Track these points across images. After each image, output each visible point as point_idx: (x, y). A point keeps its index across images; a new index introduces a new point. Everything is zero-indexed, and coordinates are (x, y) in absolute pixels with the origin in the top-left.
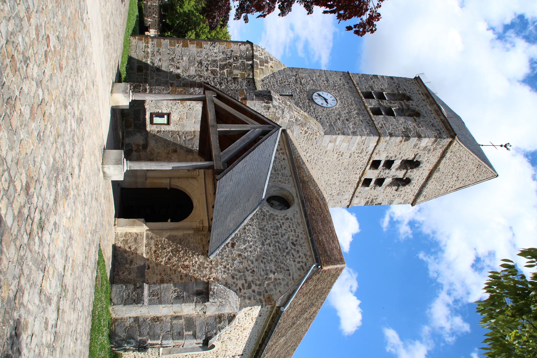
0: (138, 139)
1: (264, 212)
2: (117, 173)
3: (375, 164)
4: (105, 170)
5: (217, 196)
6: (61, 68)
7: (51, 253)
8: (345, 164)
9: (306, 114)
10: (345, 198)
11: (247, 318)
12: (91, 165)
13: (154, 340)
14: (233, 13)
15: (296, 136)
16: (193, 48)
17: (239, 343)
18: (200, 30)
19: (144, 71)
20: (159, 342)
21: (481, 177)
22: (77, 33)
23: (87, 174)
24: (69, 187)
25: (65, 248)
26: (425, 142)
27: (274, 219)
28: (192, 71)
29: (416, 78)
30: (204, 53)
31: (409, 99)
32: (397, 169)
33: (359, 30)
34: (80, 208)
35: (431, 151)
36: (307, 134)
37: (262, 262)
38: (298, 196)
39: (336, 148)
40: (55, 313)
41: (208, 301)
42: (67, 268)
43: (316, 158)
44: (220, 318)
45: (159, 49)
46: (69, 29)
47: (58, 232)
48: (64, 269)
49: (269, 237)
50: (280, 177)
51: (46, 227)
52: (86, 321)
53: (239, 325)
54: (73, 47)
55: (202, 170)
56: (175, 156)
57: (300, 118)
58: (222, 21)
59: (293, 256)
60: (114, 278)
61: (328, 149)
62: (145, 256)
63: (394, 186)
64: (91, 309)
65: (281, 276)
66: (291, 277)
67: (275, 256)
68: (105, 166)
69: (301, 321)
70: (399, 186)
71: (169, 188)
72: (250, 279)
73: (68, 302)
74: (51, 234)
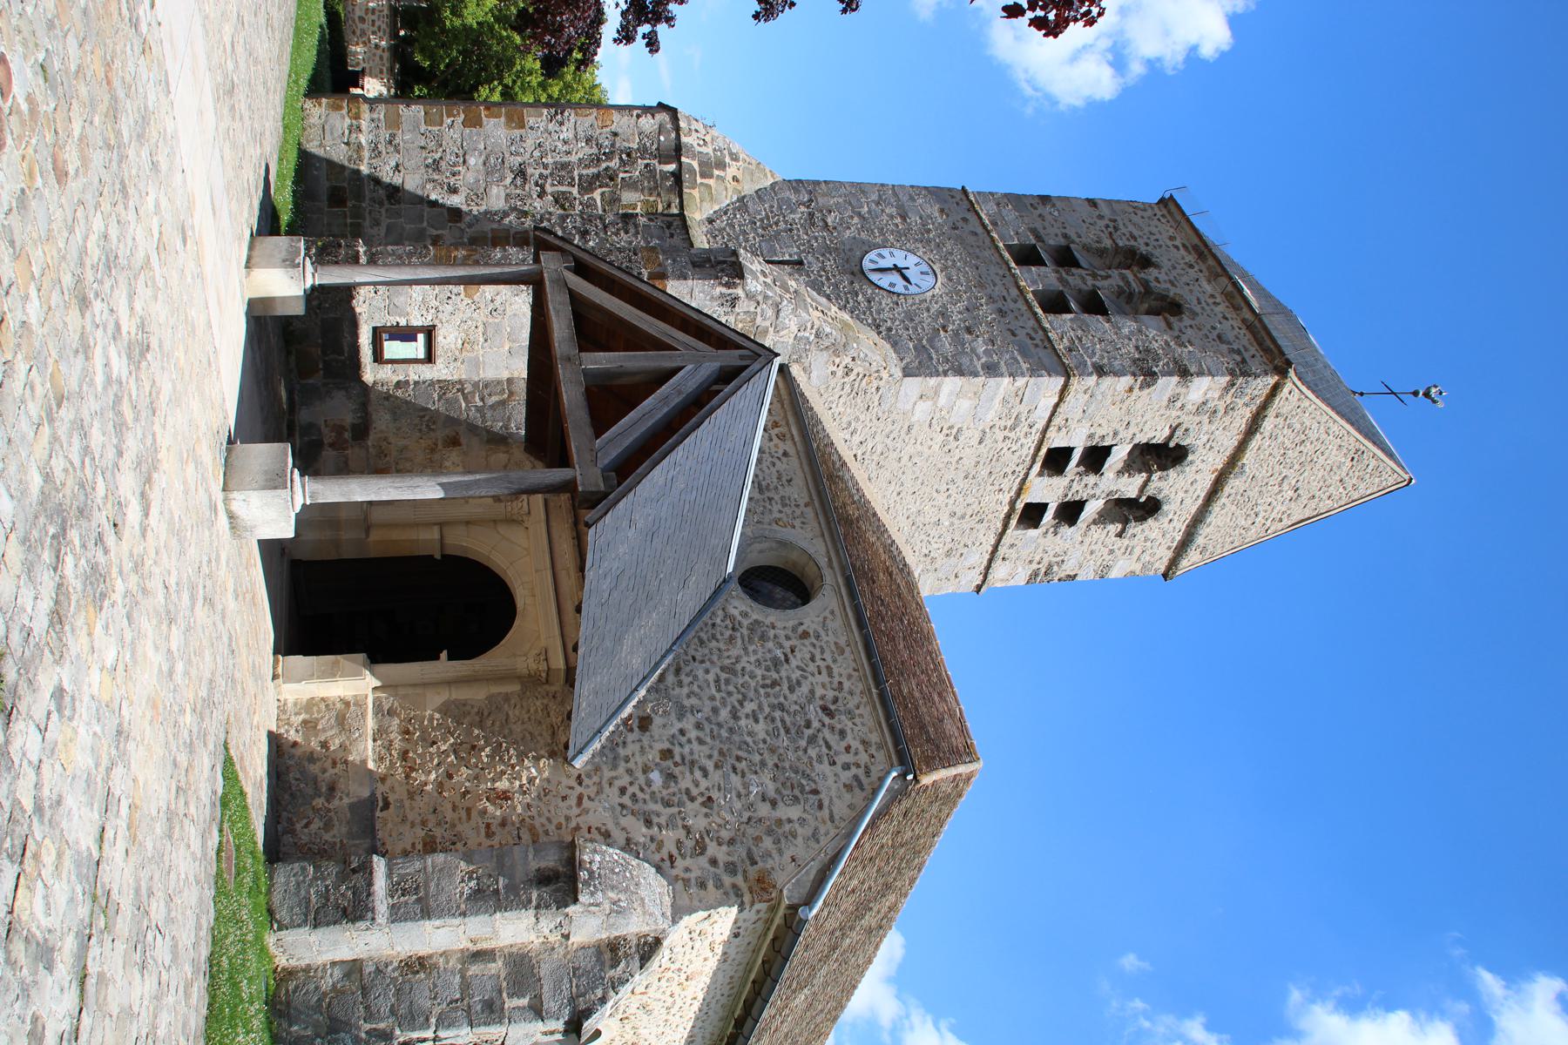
0: (338, 410)
1: (733, 618)
2: (274, 514)
3: (1056, 461)
4: (236, 507)
5: (590, 575)
6: (61, 175)
7: (46, 792)
8: (968, 463)
9: (846, 316)
10: (967, 564)
11: (697, 944)
12: (186, 492)
13: (414, 1030)
14: (610, 29)
15: (817, 381)
16: (496, 130)
17: (675, 1020)
18: (514, 82)
19: (349, 204)
20: (429, 1034)
21: (1362, 486)
22: (117, 64)
23: (171, 522)
24: (109, 565)
25: (102, 769)
26: (1203, 388)
27: (763, 638)
28: (496, 199)
29: (1162, 201)
30: (530, 143)
31: (1146, 262)
32: (1120, 473)
33: (1046, 17)
34: (150, 634)
35: (1220, 414)
36: (853, 376)
37: (734, 769)
38: (835, 564)
39: (937, 416)
40: (74, 990)
41: (576, 900)
42: (109, 834)
43: (879, 448)
44: (611, 951)
45: (393, 136)
46: (88, 47)
47: (71, 719)
48: (101, 838)
49: (751, 694)
50: (776, 507)
51: (22, 707)
52: (187, 995)
53: (673, 967)
54: (102, 108)
55: (539, 499)
56: (454, 456)
57: (828, 330)
58: (580, 49)
59: (829, 747)
60: (278, 841)
61: (914, 419)
62: (371, 765)
63: (1112, 522)
64: (205, 952)
65: (794, 812)
66: (826, 812)
67: (772, 750)
68: (235, 495)
69: (854, 935)
70: (1126, 522)
71: (438, 556)
72: (698, 823)
73: (121, 947)
74: (43, 730)
